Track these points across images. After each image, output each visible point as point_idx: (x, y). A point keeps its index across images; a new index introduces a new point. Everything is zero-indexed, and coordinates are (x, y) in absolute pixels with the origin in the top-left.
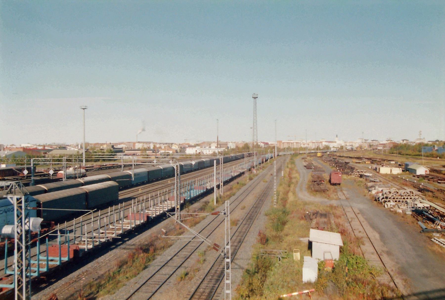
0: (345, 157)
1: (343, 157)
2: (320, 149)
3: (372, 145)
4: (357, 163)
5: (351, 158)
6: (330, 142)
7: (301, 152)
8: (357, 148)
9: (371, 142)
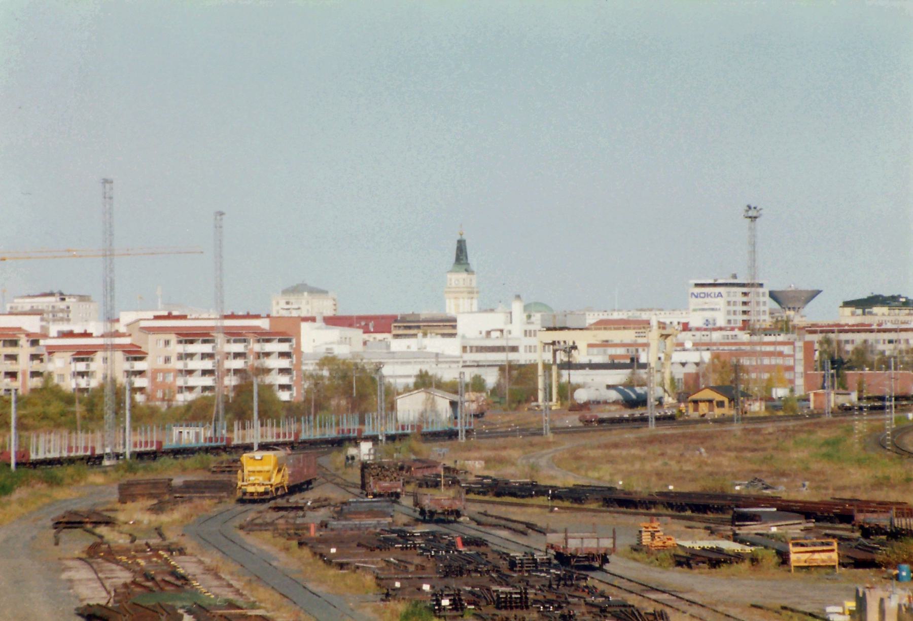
0: (558, 495)
1: (528, 491)
2: (270, 411)
3: (862, 358)
4: (686, 560)
5: (625, 502)
6: (382, 324)
7: (48, 446)
8: (687, 390)
9: (848, 317)
